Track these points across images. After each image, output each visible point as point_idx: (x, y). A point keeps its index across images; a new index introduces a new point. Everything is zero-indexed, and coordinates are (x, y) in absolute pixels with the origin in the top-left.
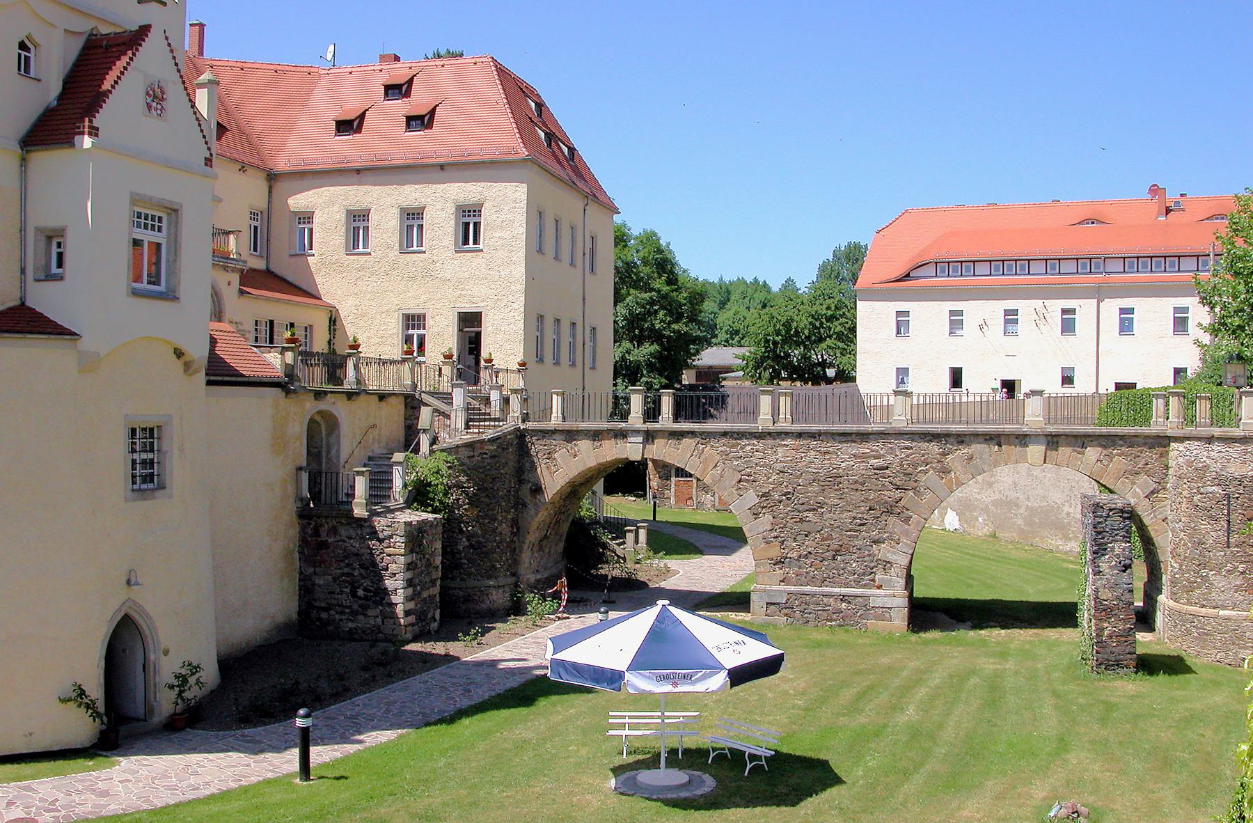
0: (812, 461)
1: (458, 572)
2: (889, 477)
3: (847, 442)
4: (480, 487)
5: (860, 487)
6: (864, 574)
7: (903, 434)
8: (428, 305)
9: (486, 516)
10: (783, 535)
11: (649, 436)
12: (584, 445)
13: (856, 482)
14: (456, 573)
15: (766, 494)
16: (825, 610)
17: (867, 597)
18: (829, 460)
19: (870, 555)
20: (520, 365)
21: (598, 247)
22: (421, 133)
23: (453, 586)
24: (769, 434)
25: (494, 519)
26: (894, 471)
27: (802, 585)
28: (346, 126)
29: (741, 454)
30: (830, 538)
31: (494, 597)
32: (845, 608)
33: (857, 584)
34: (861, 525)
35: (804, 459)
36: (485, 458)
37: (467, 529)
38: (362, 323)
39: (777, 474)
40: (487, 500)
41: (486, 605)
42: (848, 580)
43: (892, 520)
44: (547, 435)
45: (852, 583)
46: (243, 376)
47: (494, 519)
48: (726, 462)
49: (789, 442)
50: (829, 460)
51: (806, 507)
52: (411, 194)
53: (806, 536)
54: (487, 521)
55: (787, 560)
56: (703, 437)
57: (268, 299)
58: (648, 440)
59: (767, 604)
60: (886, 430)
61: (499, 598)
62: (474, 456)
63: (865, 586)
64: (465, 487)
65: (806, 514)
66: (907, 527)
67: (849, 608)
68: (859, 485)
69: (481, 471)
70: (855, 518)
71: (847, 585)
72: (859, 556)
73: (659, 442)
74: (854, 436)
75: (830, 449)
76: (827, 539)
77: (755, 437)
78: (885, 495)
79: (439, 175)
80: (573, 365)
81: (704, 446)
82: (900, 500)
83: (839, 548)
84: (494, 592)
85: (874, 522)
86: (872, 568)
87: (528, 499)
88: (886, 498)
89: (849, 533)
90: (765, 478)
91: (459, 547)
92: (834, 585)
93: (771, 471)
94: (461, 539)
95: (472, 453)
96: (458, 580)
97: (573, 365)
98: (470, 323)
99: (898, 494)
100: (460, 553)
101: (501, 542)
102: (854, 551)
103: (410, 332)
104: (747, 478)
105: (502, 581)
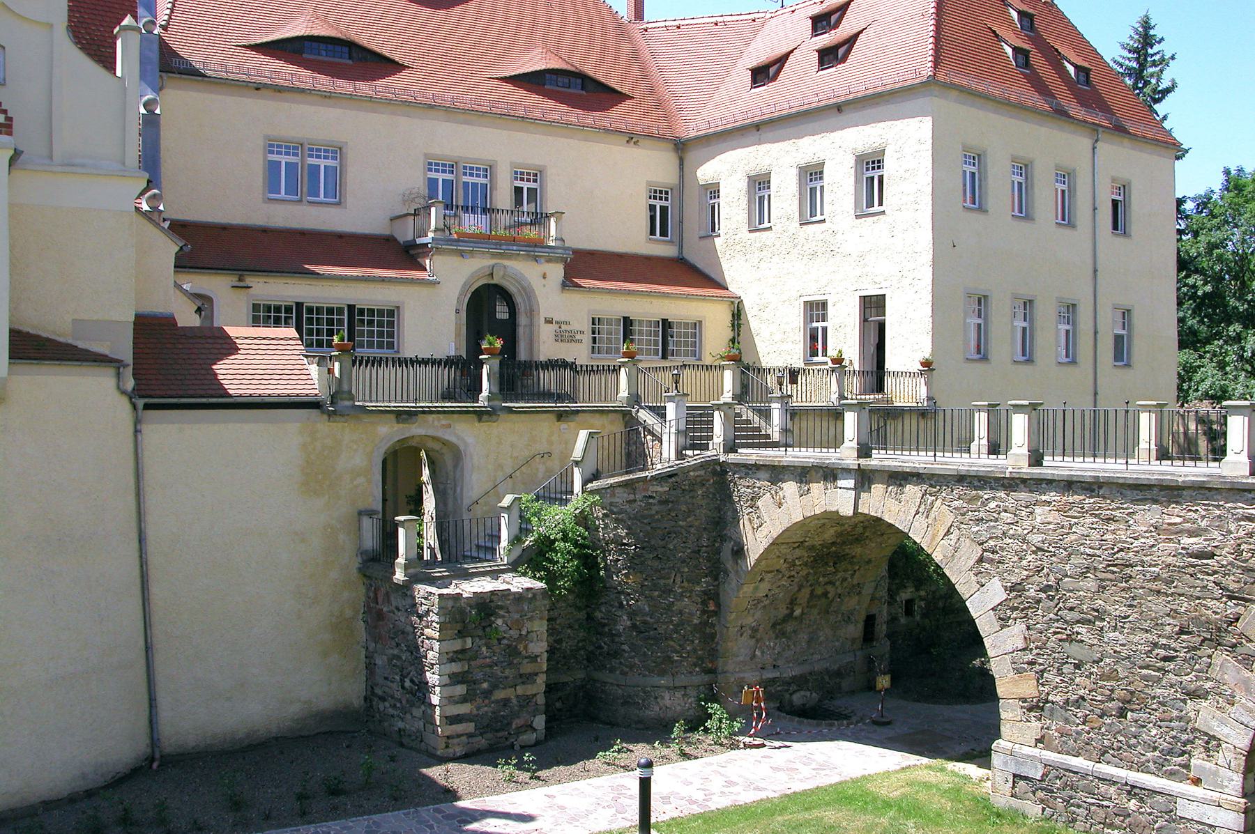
0: (1085, 533)
1: (617, 661)
2: (1215, 572)
3: (1143, 501)
4: (645, 544)
5: (1163, 588)
6: (1170, 752)
7: (1245, 490)
8: (828, 289)
9: (655, 586)
10: (1041, 661)
11: (864, 479)
12: (790, 488)
13: (1156, 578)
14: (615, 662)
15: (1018, 587)
16: (1103, 806)
17: (1171, 797)
18: (1114, 532)
19: (1180, 719)
20: (923, 364)
21: (1132, 197)
22: (833, 69)
23: (610, 680)
24: (1024, 481)
25: (667, 591)
26: (1225, 563)
27: (1068, 753)
28: (762, 74)
29: (982, 514)
30: (1112, 675)
31: (668, 702)
32: (1134, 809)
33: (1159, 768)
34: (1165, 659)
35: (1074, 530)
36: (651, 503)
37: (628, 604)
38: (765, 316)
39: (1034, 552)
40: (656, 564)
41: (653, 711)
42: (1144, 758)
43: (1220, 657)
44: (750, 472)
45: (1151, 764)
46: (230, 396)
47: (667, 591)
48: (963, 526)
49: (1051, 496)
50: (1114, 532)
51: (1075, 615)
52: (809, 147)
53: (1077, 666)
54: (657, 593)
55: (1048, 705)
56: (933, 482)
57: (649, 294)
58: (863, 486)
59: (1015, 776)
60: (1208, 482)
61: (672, 702)
62: (635, 501)
63: (1171, 775)
64: (625, 544)
65: (1077, 628)
66: (1247, 674)
67: (1143, 810)
68: (1164, 583)
69: (645, 521)
70: (1155, 645)
71: (1142, 768)
72: (1163, 716)
73: (878, 489)
74: (1156, 491)
75: (1117, 513)
76: (1109, 679)
77: (1003, 485)
78: (1208, 608)
79: (836, 119)
80: (1072, 360)
81: (934, 498)
82: (1237, 620)
83: (1128, 697)
84: (667, 696)
85: (1188, 656)
86: (1185, 744)
87: (729, 565)
88: (1209, 612)
89: (1144, 672)
90: (1016, 559)
91: (618, 627)
92: (1121, 762)
93: (1025, 547)
94: (620, 616)
95: (632, 497)
96: (618, 672)
97: (1072, 360)
98: (873, 307)
99: (1232, 608)
100: (619, 635)
101: (681, 624)
102: (1154, 706)
103: (815, 324)
104: (991, 556)
105: (682, 680)
